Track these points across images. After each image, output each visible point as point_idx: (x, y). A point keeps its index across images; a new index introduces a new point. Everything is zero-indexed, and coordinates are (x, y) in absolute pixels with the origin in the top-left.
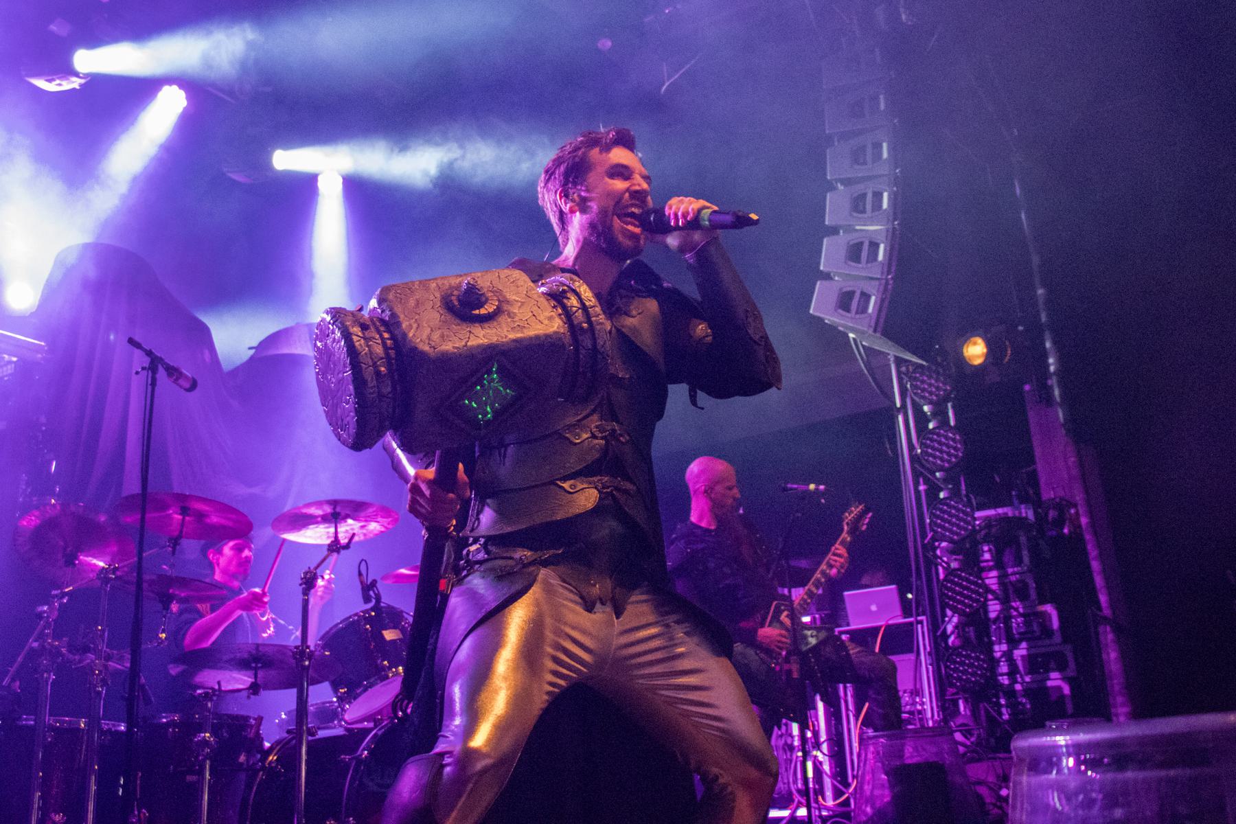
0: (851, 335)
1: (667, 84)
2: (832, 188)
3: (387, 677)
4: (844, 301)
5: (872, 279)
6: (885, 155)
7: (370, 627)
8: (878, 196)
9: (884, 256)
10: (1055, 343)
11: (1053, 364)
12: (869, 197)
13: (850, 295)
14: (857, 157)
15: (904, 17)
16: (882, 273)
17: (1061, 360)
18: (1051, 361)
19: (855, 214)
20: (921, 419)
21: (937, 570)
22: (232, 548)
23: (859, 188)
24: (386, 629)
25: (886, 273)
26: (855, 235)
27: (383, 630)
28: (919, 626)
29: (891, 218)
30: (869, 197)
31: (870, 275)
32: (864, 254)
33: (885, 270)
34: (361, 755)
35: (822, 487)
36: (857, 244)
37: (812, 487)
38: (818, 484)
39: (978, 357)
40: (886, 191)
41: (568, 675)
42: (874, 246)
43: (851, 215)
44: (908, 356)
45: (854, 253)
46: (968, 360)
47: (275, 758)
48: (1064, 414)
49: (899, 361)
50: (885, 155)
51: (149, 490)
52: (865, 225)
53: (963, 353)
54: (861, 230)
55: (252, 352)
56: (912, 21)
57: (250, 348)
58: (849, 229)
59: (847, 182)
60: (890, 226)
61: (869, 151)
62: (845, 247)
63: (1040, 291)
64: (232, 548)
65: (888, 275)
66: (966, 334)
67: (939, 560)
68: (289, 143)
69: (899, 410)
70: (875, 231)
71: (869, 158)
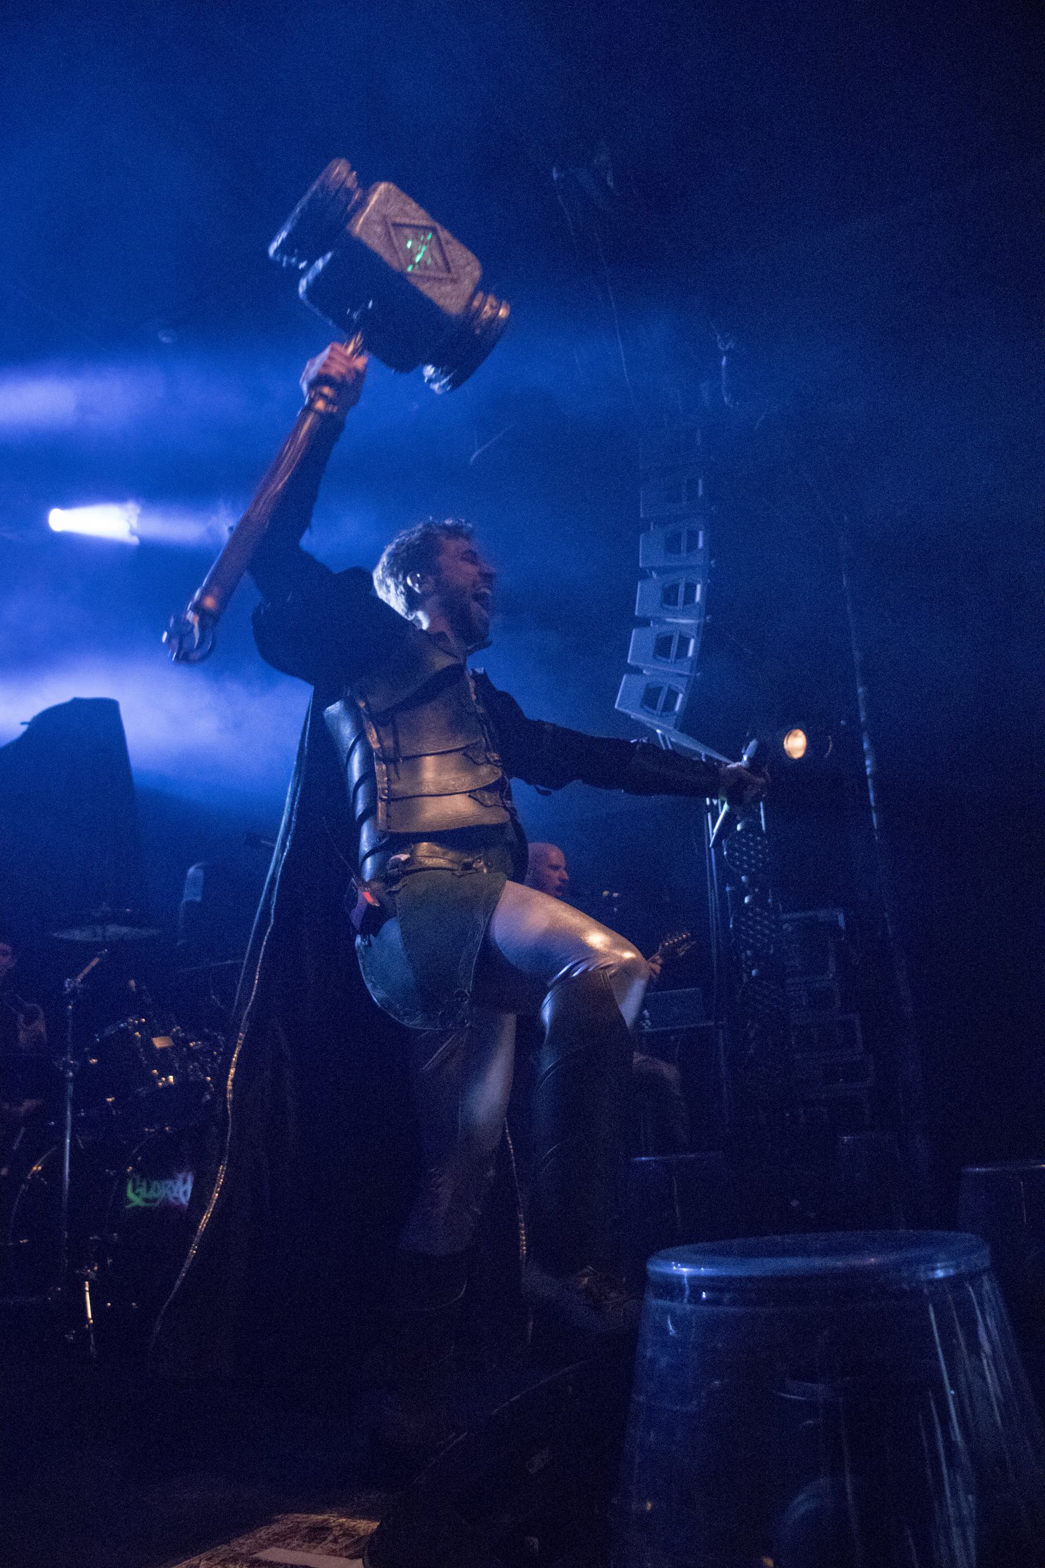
0: (659, 731)
2: (644, 575)
4: (650, 698)
6: (701, 544)
8: (691, 588)
9: (694, 651)
10: (872, 743)
11: (869, 767)
12: (682, 589)
13: (657, 690)
14: (672, 545)
15: (726, 399)
16: (691, 671)
17: (878, 762)
18: (868, 763)
19: (666, 606)
24: (156, 1037)
27: (153, 1037)
29: (703, 614)
30: (682, 589)
31: (679, 672)
32: (674, 649)
35: (615, 895)
36: (666, 638)
39: (798, 750)
42: (684, 642)
43: (662, 606)
45: (663, 647)
46: (788, 754)
47: (40, 1168)
50: (701, 544)
53: (783, 745)
54: (671, 624)
55: (25, 728)
57: (23, 723)
58: (660, 621)
59: (661, 571)
60: (703, 620)
63: (860, 690)
68: (66, 502)
70: (686, 625)
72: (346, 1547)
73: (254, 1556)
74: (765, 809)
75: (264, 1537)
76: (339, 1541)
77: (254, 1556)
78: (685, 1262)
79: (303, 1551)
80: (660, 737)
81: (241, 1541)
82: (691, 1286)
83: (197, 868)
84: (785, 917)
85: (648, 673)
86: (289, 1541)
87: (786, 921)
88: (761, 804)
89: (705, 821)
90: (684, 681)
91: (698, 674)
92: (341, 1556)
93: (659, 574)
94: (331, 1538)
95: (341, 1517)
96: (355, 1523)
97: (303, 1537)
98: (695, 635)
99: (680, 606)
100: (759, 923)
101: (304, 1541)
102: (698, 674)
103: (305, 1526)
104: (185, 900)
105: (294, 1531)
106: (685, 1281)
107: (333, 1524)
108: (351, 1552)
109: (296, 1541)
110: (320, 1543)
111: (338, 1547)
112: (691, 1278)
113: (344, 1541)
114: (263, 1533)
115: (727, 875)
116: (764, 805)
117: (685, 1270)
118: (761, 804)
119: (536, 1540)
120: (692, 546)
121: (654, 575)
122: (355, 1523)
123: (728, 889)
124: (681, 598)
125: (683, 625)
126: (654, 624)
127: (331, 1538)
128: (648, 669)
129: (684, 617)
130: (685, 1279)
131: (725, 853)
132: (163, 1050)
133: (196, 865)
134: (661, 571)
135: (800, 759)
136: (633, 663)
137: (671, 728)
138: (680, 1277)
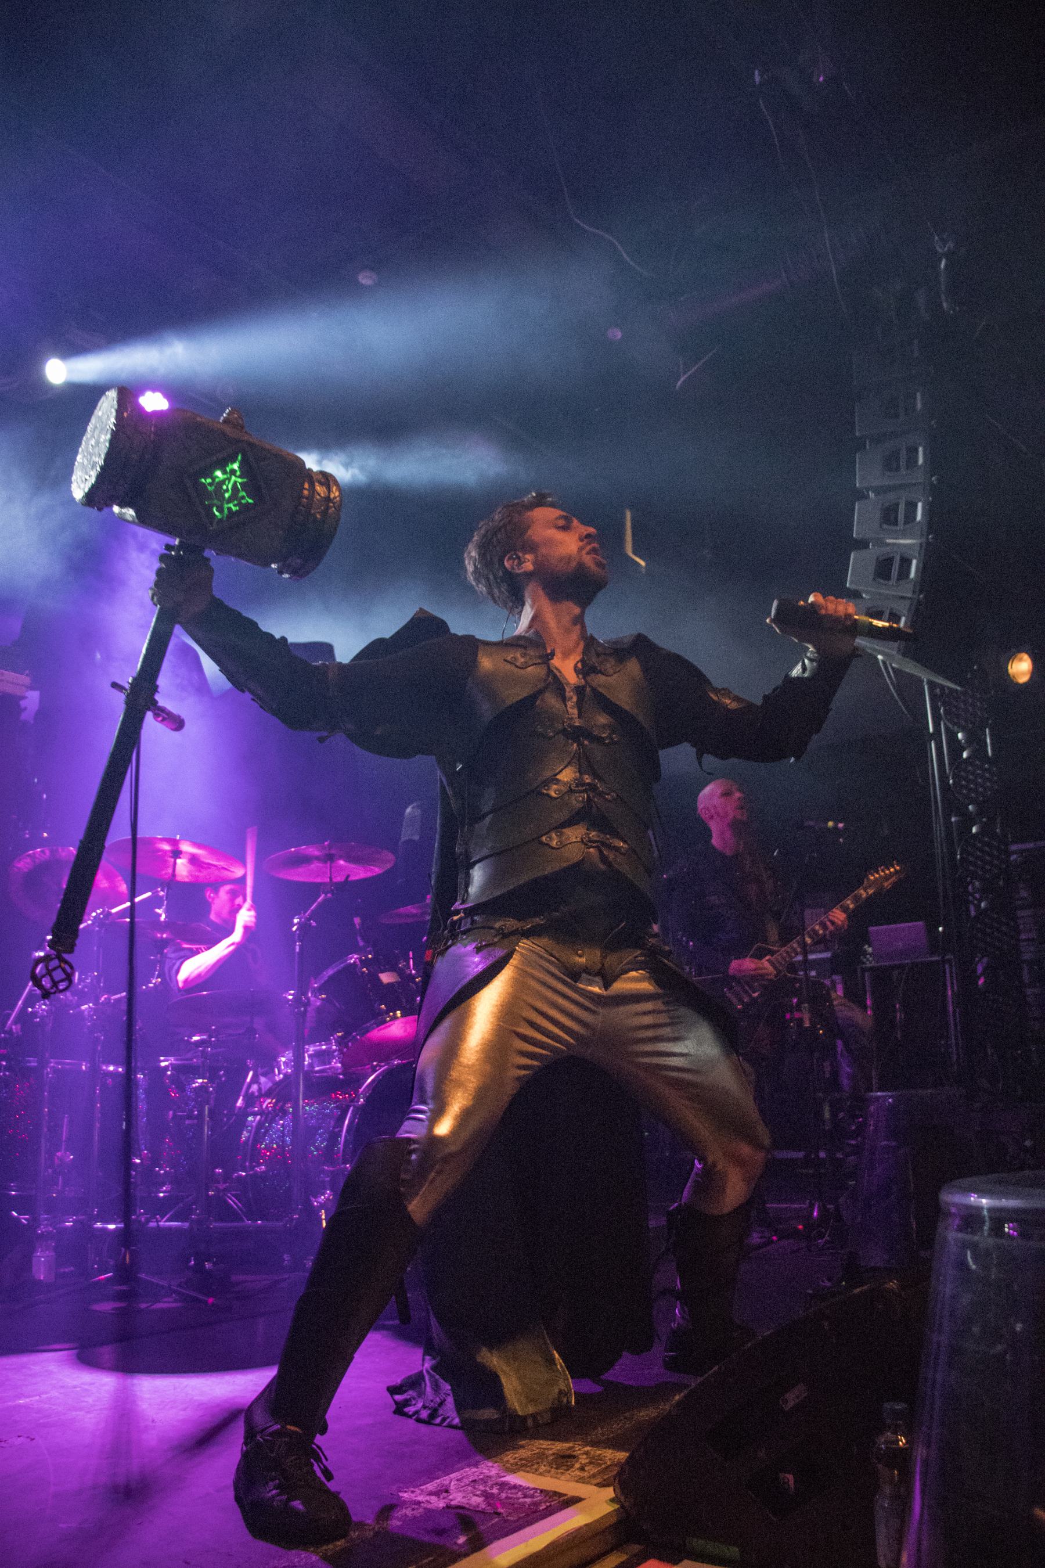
0: (880, 657)
1: (682, 379)
2: (861, 496)
3: (385, 1022)
5: (903, 598)
6: (921, 461)
7: (367, 969)
8: (911, 506)
12: (902, 508)
14: (891, 463)
15: (945, 305)
16: (914, 592)
19: (885, 526)
20: (956, 748)
21: (968, 909)
22: (228, 892)
23: (891, 496)
25: (917, 593)
26: (885, 550)
28: (947, 966)
30: (902, 508)
31: (900, 594)
33: (918, 588)
34: (29, 1062)
35: (841, 825)
37: (830, 824)
38: (837, 821)
39: (1023, 674)
40: (920, 501)
41: (541, 1055)
42: (906, 562)
44: (940, 681)
45: (883, 569)
48: (174, 1308)
49: (932, 685)
51: (140, 835)
52: (896, 539)
54: (894, 544)
56: (954, 310)
58: (880, 543)
60: (924, 540)
61: (903, 454)
62: (874, 562)
64: (228, 892)
65: (920, 594)
66: (1011, 651)
67: (971, 898)
69: (932, 737)
71: (903, 463)
72: (594, 1476)
73: (503, 1479)
74: (991, 736)
75: (512, 1461)
76: (587, 1468)
77: (503, 1479)
78: (982, 1193)
79: (551, 1477)
80: (881, 663)
81: (490, 1464)
82: (991, 1219)
83: (413, 808)
84: (1014, 847)
85: (868, 597)
86: (535, 1466)
87: (1015, 852)
88: (987, 730)
89: (929, 753)
90: (908, 603)
91: (921, 596)
92: (588, 1483)
93: (877, 494)
94: (577, 1465)
95: (586, 1446)
96: (600, 1452)
97: (550, 1464)
98: (917, 555)
99: (901, 526)
100: (977, 858)
101: (552, 1467)
102: (921, 596)
103: (551, 1452)
104: (403, 839)
105: (541, 1456)
106: (985, 1213)
107: (579, 1452)
108: (598, 1480)
109: (543, 1467)
110: (567, 1470)
111: (586, 1474)
112: (991, 1210)
113: (592, 1470)
114: (510, 1457)
115: (952, 804)
116: (990, 731)
117: (984, 1201)
118: (987, 730)
119: (791, 1478)
120: (912, 461)
121: (872, 495)
122: (600, 1452)
123: (953, 819)
124: (901, 517)
125: (905, 545)
126: (873, 545)
127: (577, 1465)
128: (867, 592)
129: (905, 537)
130: (985, 1210)
131: (951, 781)
132: (390, 985)
133: (415, 804)
134: (878, 491)
135: (1025, 684)
136: (854, 587)
137: (894, 653)
138: (980, 1209)
